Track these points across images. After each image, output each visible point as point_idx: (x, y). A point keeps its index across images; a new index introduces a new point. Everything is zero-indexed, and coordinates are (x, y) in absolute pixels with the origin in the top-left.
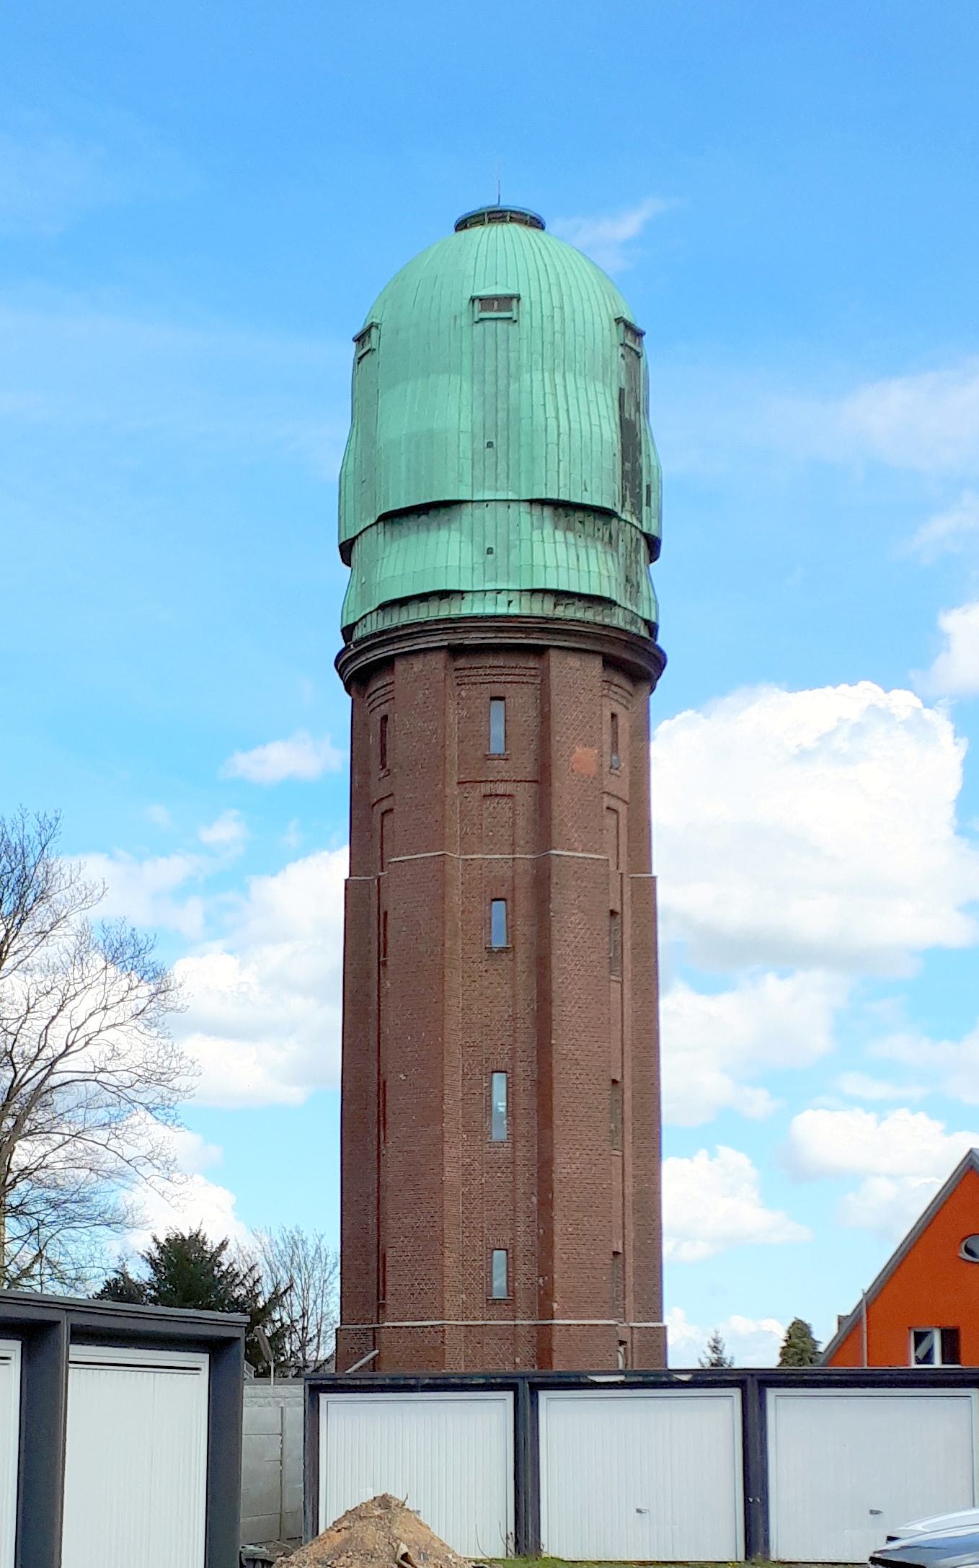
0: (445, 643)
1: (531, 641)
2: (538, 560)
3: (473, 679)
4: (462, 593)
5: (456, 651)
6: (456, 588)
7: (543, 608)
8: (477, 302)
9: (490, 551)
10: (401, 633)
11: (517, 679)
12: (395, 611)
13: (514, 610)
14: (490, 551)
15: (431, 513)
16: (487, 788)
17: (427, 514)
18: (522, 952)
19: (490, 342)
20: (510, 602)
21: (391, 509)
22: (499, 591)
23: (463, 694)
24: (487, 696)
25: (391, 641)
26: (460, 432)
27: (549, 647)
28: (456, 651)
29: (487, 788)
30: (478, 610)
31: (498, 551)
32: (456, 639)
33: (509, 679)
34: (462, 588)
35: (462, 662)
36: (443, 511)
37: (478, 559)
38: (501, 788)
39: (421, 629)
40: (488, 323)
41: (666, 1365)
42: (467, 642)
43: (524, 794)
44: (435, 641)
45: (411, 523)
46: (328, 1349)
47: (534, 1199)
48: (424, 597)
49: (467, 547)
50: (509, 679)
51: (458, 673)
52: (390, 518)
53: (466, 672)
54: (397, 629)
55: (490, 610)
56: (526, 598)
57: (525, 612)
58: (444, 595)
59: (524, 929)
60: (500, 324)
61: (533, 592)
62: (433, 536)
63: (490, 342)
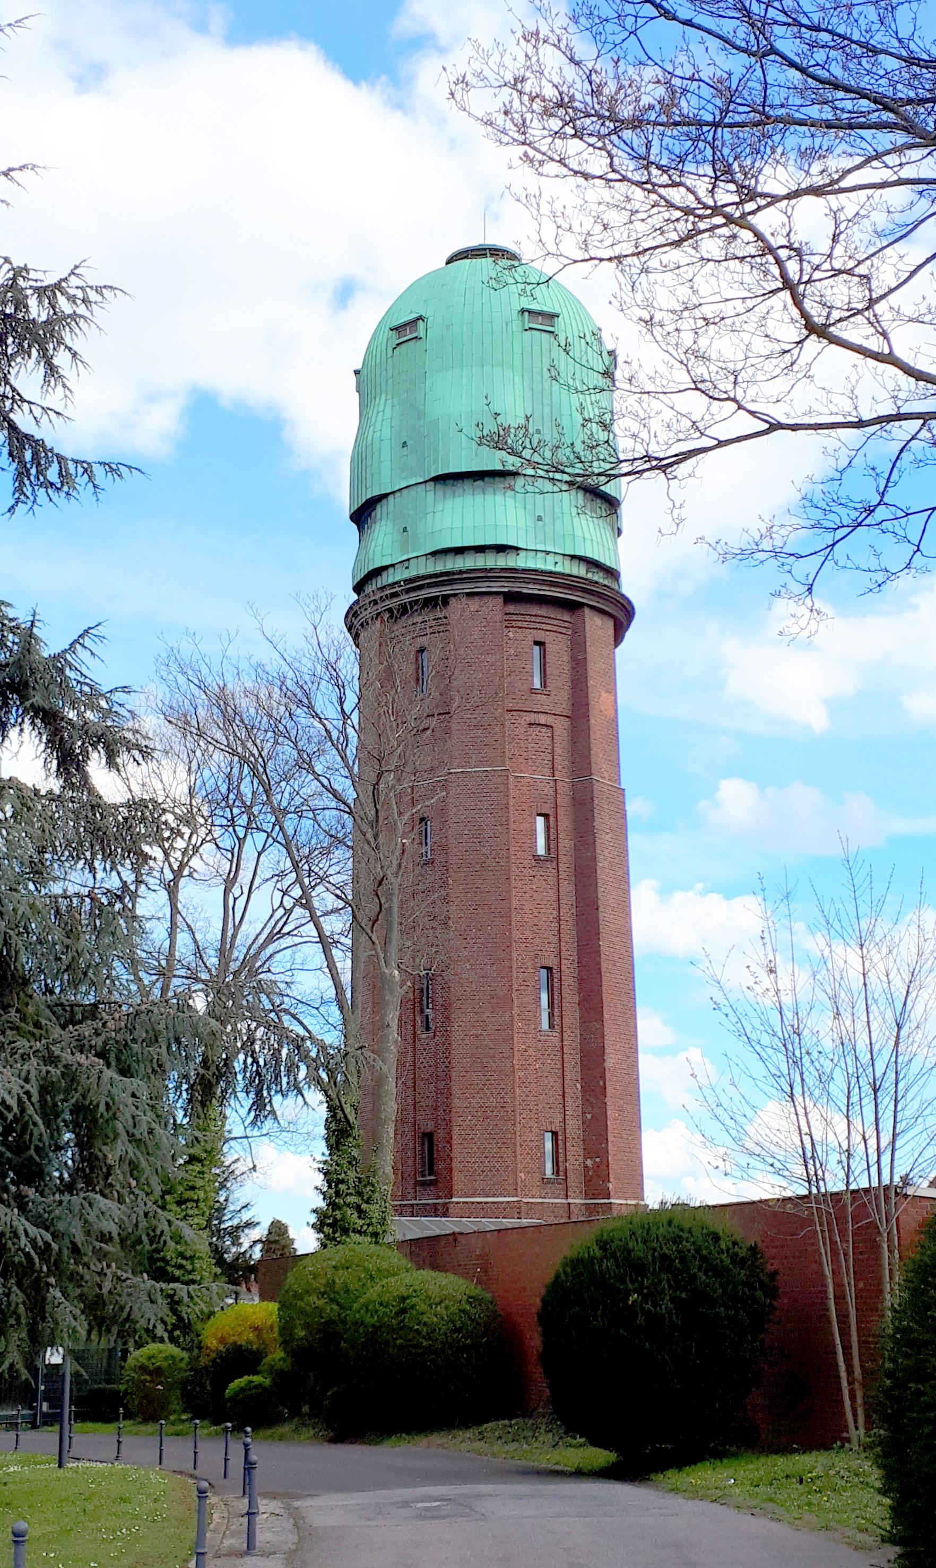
0: (506, 590)
1: (575, 598)
2: (578, 532)
3: (520, 624)
4: (517, 549)
5: (510, 598)
6: (515, 545)
7: (579, 570)
8: (526, 314)
9: (540, 519)
10: (464, 576)
11: (555, 628)
12: (450, 557)
13: (559, 569)
14: (540, 519)
15: (486, 479)
16: (532, 718)
17: (483, 480)
18: (565, 861)
19: (536, 348)
20: (556, 563)
21: (440, 473)
22: (548, 553)
23: (511, 635)
24: (531, 639)
25: (451, 582)
26: (516, 416)
27: (582, 605)
28: (510, 598)
29: (532, 718)
30: (531, 565)
31: (547, 519)
32: (516, 587)
33: (549, 627)
34: (520, 546)
35: (511, 608)
36: (497, 479)
37: (530, 523)
38: (543, 719)
39: (487, 574)
40: (534, 332)
41: (639, 1192)
42: (525, 591)
43: (561, 727)
44: (496, 587)
45: (468, 484)
46: (46, 655)
47: (579, 1086)
48: (481, 549)
49: (521, 512)
50: (549, 627)
51: (507, 617)
52: (443, 479)
53: (514, 617)
54: (461, 572)
55: (540, 566)
56: (567, 562)
57: (567, 571)
58: (501, 549)
59: (566, 843)
60: (544, 334)
61: (573, 557)
62: (489, 498)
63: (536, 348)
